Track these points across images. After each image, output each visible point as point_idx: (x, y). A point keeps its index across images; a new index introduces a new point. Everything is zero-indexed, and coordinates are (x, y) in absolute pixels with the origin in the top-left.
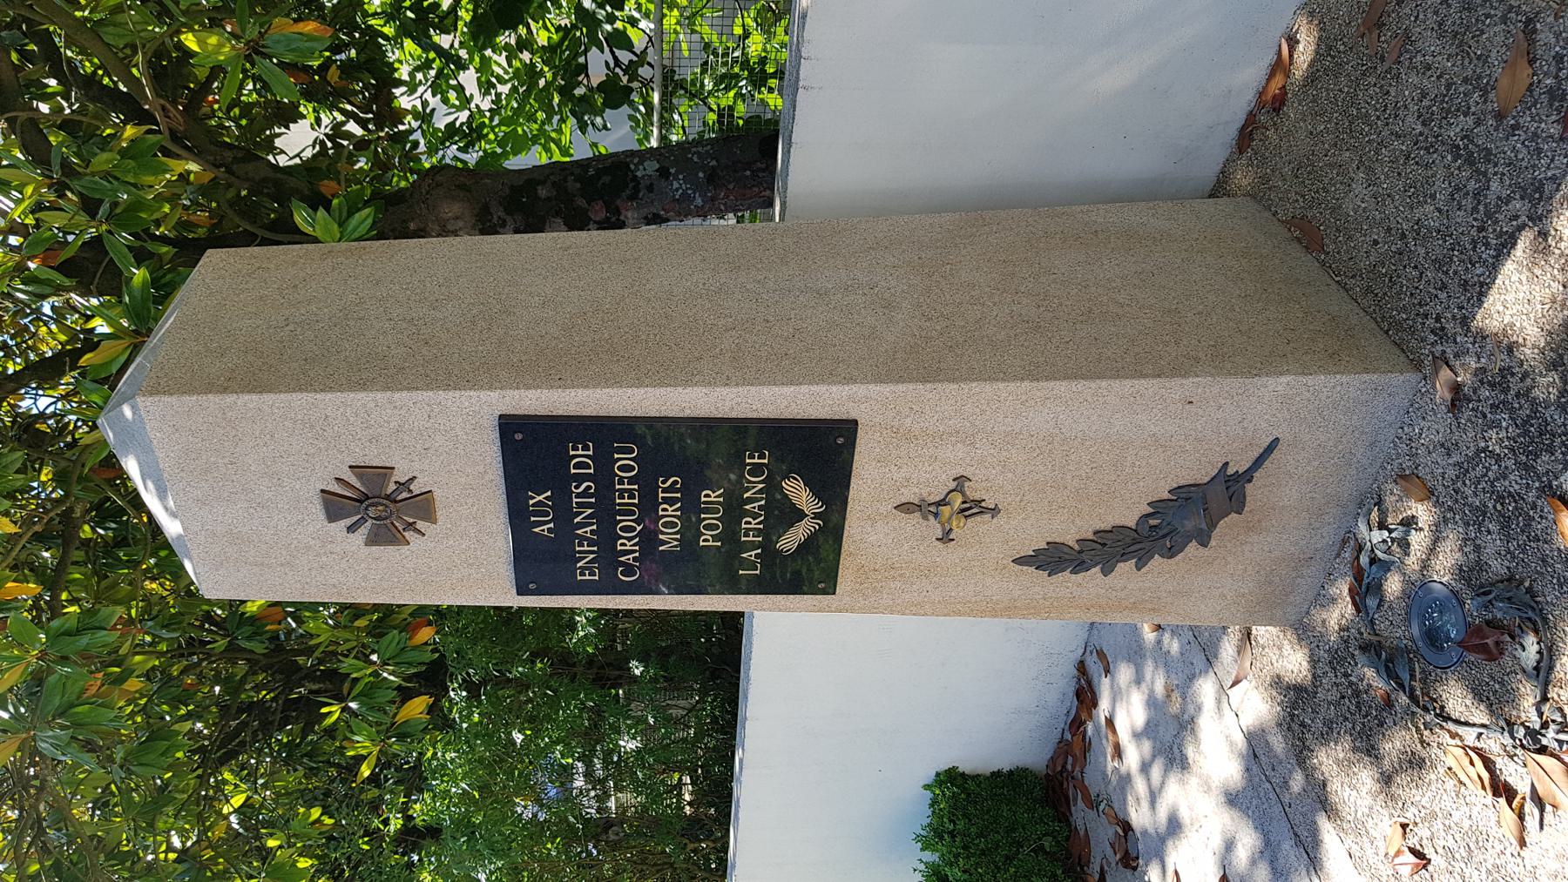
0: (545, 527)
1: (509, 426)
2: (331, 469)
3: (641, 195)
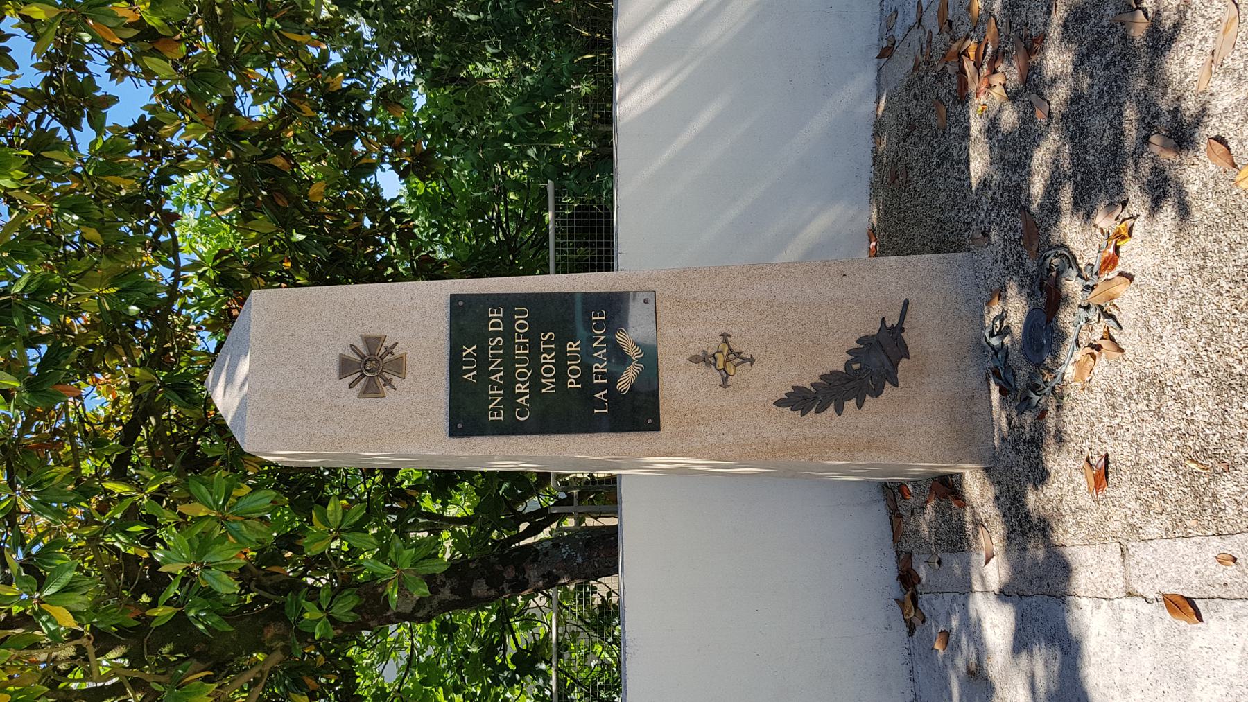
0: (471, 374)
1: (454, 298)
2: (347, 340)
3: (540, 559)
